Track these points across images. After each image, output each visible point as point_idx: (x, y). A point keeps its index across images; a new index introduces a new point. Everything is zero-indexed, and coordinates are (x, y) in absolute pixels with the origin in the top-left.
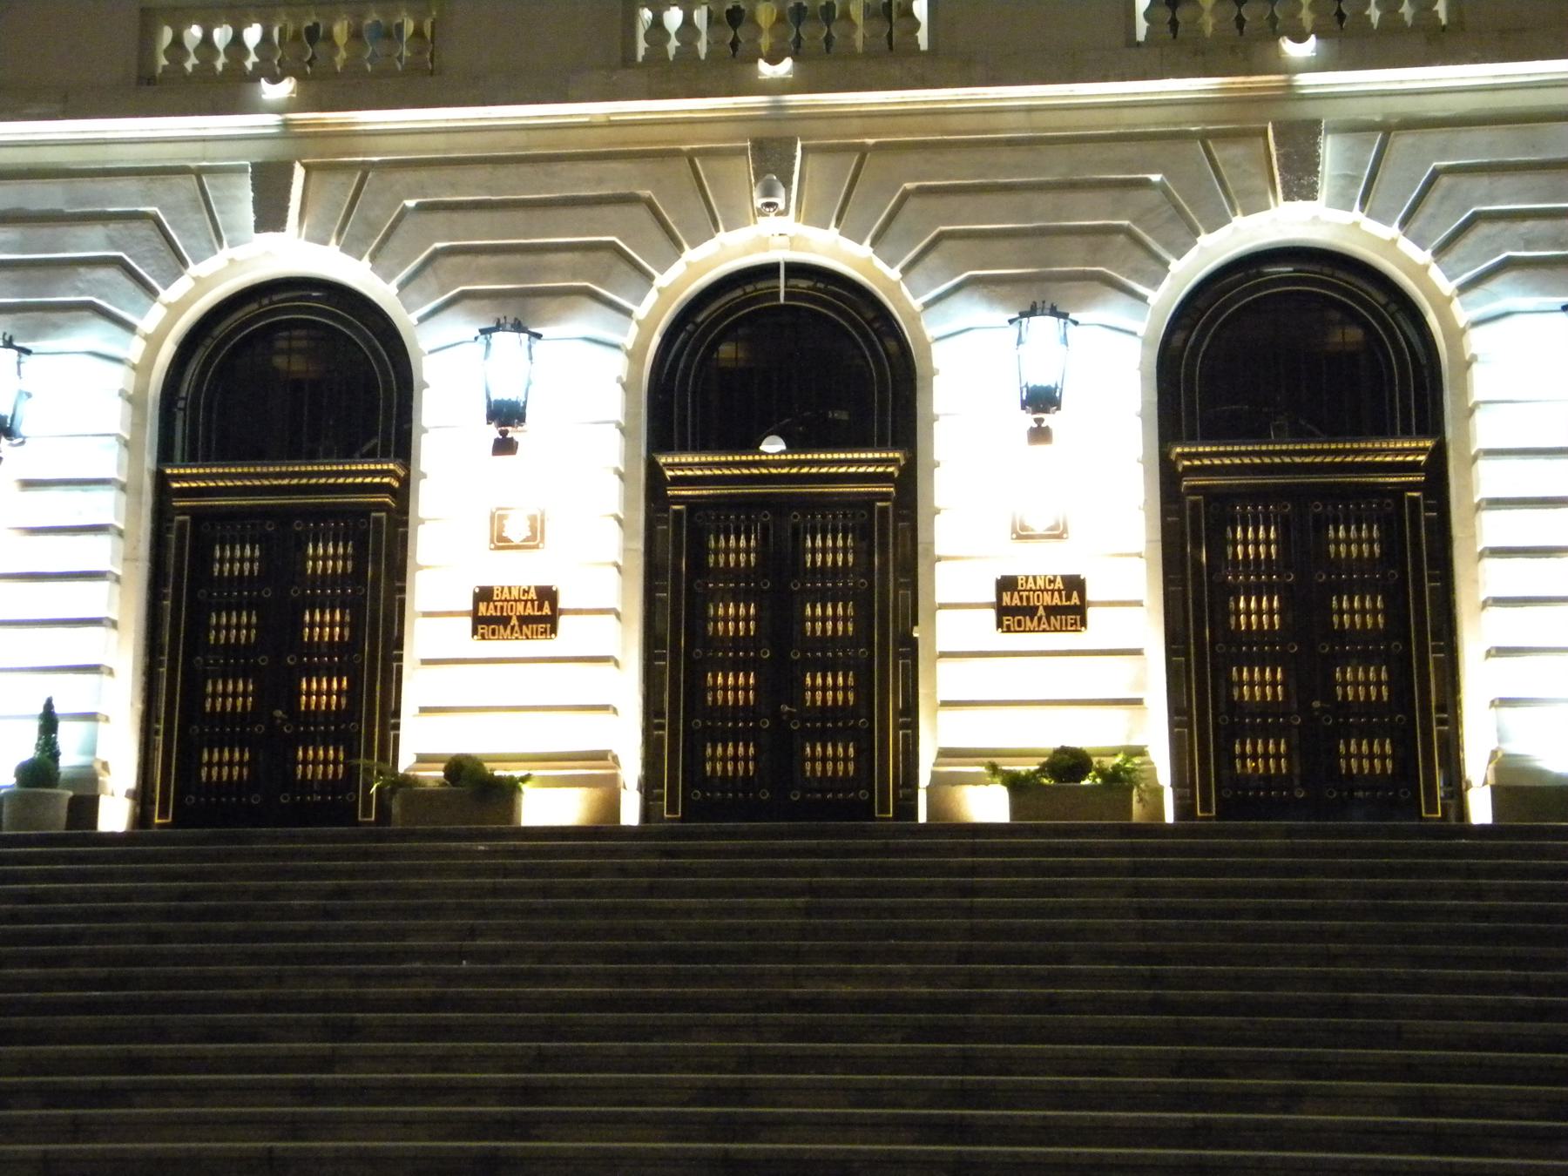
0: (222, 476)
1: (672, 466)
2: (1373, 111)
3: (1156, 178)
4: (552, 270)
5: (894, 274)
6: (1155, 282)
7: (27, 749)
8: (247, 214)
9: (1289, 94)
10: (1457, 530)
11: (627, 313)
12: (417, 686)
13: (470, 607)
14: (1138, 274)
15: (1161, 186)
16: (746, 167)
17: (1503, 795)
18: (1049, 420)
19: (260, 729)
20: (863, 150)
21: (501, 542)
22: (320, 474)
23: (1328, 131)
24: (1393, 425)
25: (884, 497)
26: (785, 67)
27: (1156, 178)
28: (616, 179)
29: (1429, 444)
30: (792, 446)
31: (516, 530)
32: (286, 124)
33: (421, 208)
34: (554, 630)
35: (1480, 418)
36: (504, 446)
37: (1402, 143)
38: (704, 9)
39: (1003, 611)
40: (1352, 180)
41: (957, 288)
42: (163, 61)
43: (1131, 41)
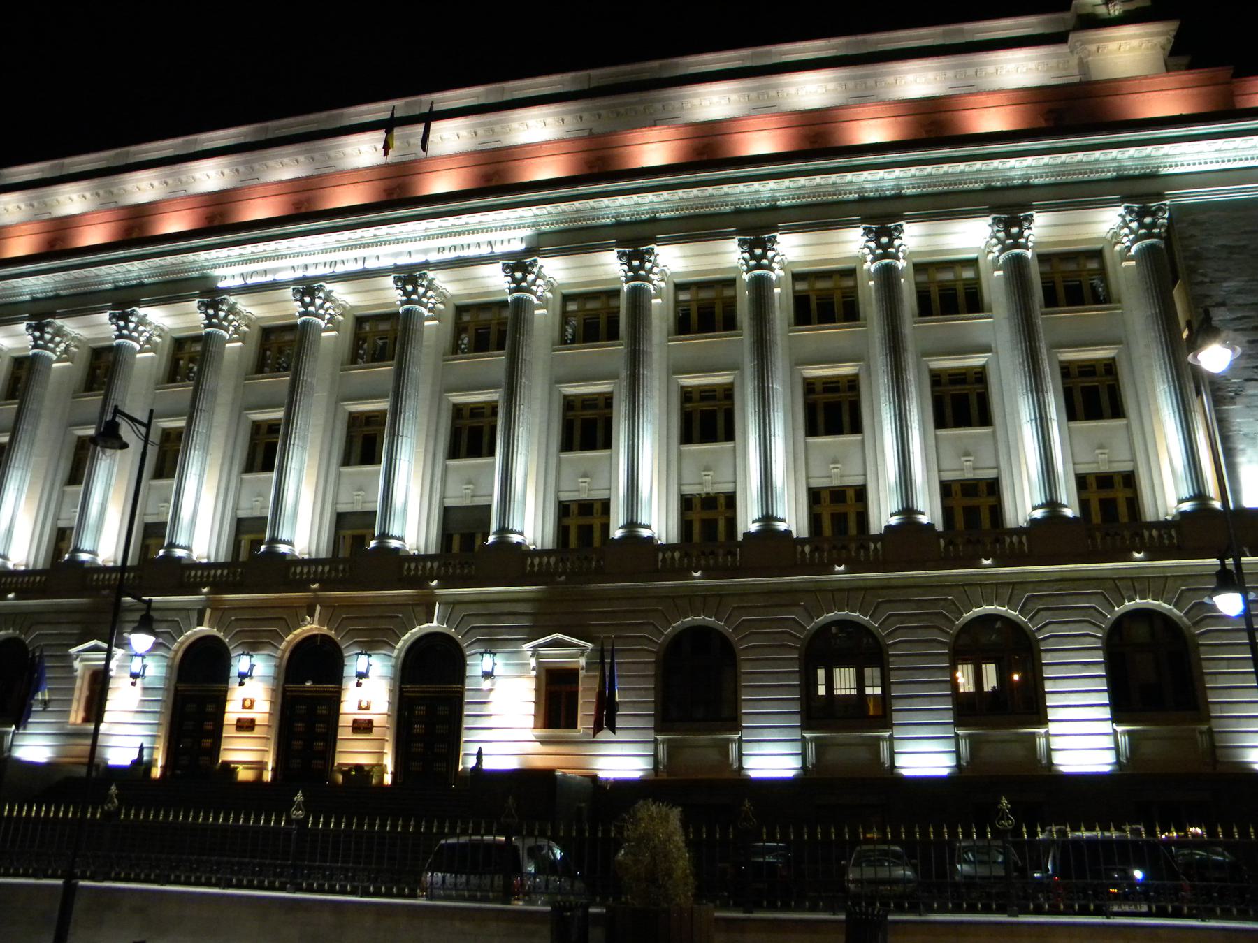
2: (451, 599)
7: (135, 757)
8: (196, 622)
12: (340, 747)
18: (363, 681)
20: (335, 606)
21: (244, 707)
26: (842, 568)
30: (314, 683)
31: (364, 705)
32: (208, 598)
33: (236, 620)
37: (457, 607)
42: (405, 573)
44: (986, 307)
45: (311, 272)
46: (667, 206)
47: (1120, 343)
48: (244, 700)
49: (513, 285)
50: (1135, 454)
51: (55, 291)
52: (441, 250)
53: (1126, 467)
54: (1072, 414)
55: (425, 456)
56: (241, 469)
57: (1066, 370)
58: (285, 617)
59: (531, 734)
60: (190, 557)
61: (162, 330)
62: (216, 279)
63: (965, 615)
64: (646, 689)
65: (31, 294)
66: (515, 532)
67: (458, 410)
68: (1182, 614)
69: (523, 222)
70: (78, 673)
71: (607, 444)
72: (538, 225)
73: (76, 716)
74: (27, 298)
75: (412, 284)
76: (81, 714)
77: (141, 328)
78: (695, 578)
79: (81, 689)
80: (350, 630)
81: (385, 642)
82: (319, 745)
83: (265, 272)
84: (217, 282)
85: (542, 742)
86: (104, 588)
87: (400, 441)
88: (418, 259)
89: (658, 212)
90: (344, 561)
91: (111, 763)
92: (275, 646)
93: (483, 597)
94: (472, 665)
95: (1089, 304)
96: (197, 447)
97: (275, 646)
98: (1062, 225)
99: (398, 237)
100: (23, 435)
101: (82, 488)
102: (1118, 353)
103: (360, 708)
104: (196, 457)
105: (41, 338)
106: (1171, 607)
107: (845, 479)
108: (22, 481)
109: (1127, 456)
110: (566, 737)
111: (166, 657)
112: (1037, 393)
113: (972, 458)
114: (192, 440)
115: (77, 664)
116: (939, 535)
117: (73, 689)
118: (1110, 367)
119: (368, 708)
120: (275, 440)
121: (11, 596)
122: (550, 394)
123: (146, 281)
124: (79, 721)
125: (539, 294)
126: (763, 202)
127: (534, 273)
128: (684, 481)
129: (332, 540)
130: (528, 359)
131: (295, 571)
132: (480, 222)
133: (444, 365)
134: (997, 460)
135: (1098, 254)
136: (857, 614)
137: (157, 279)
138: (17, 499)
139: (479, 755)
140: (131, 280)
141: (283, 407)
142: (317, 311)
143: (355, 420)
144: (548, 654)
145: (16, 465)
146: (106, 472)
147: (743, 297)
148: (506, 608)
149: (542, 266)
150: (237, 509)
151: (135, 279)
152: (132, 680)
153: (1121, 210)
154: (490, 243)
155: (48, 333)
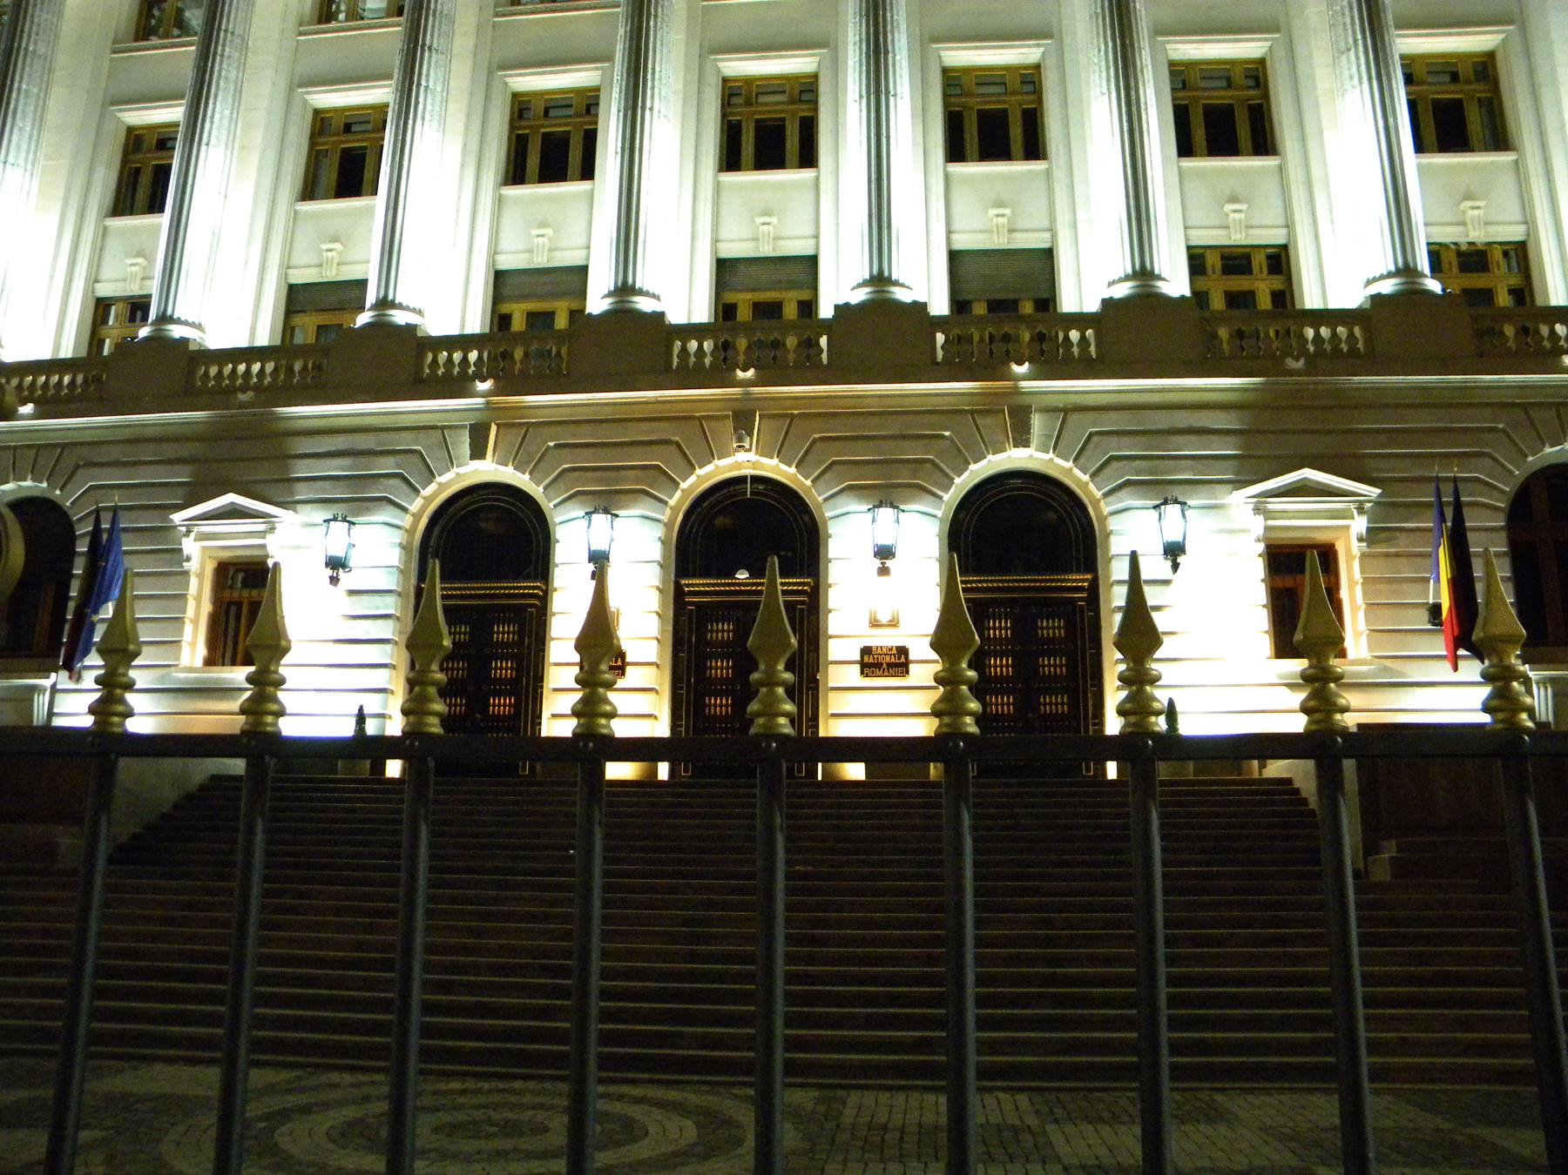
0: (718, 585)
1: (688, 586)
2: (1059, 402)
3: (947, 434)
5: (808, 483)
6: (946, 490)
9: (1017, 391)
10: (1103, 624)
11: (665, 503)
14: (936, 484)
20: (792, 417)
25: (802, 603)
26: (751, 373)
27: (947, 434)
29: (1089, 577)
32: (488, 403)
37: (1074, 418)
50: (1292, 215)
53: (1276, 237)
56: (500, 178)
57: (1182, 76)
67: (521, 106)
70: (192, 566)
76: (202, 651)
79: (198, 599)
80: (834, 463)
82: (501, 705)
86: (244, 389)
90: (304, 351)
91: (617, 735)
92: (934, 495)
96: (427, 117)
97: (934, 495)
100: (21, 102)
101: (164, 220)
107: (783, 243)
113: (1007, 211)
114: (417, 103)
115: (190, 546)
116: (939, 323)
118: (1256, 74)
119: (894, 623)
120: (594, 127)
122: (289, 102)
124: (199, 662)
128: (295, 261)
131: (206, 373)
133: (112, 60)
143: (135, 140)
148: (1181, 419)
152: (329, 572)
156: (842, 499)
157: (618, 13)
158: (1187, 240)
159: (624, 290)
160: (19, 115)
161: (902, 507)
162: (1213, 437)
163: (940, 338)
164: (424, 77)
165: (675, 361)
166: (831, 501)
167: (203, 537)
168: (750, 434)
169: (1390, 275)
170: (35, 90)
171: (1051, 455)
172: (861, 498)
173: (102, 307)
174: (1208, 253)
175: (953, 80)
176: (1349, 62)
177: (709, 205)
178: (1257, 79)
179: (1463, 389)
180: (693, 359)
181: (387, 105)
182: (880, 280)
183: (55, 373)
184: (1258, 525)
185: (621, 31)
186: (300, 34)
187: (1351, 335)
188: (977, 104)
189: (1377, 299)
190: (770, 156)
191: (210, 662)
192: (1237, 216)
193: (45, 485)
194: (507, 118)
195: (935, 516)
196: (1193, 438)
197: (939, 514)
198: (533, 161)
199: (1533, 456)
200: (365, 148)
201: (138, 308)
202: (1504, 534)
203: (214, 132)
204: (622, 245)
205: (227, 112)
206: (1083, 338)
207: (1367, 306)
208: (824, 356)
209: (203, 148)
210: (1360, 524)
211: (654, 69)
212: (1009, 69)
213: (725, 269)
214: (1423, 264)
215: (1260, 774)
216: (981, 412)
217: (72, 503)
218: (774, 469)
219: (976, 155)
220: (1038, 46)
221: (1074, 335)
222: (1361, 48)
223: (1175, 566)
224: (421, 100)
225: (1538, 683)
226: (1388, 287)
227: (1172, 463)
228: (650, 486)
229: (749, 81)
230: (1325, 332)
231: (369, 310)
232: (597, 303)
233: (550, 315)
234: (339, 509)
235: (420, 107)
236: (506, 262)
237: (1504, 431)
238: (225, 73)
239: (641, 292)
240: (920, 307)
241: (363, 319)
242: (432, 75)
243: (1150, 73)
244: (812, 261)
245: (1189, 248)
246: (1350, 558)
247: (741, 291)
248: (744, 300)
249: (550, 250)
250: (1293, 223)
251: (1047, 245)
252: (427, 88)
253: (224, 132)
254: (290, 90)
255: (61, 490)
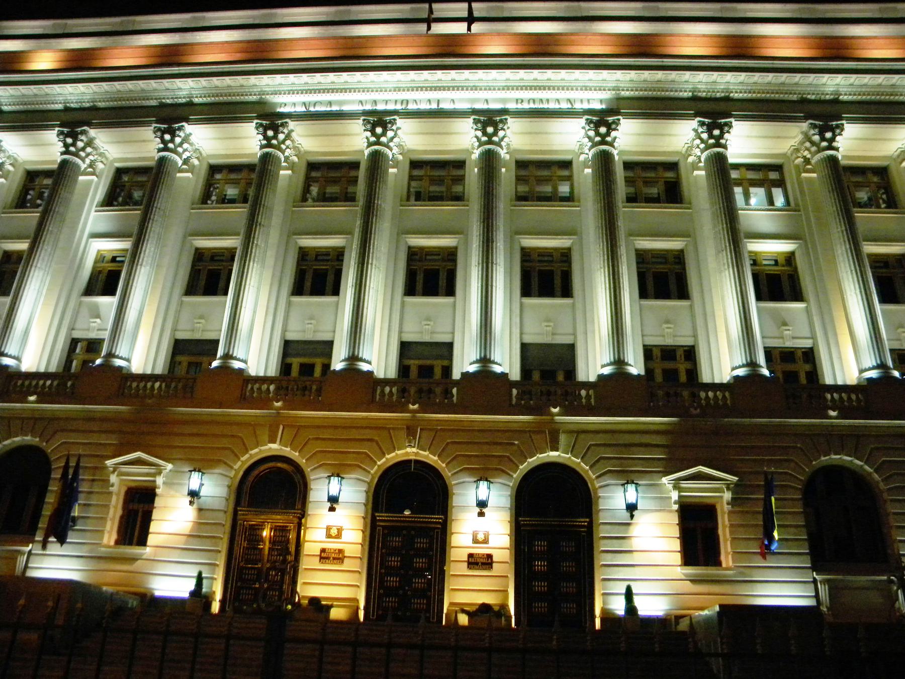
0: (395, 517)
1: (379, 516)
2: (572, 427)
3: (516, 442)
4: (636, 466)
5: (444, 465)
6: (515, 472)
9: (553, 422)
10: (595, 545)
11: (369, 472)
12: (449, 584)
13: (319, 553)
14: (510, 470)
15: (518, 445)
16: (403, 434)
17: (603, 620)
19: (401, 592)
20: (437, 431)
22: (426, 518)
23: (562, 432)
24: (382, 508)
25: (438, 528)
26: (416, 406)
27: (516, 442)
28: (368, 434)
29: (588, 520)
31: (481, 537)
34: (343, 562)
35: (601, 514)
36: (481, 514)
37: (582, 436)
38: (396, 388)
39: (321, 558)
40: (568, 445)
41: (461, 470)
43: (511, 405)
44: (576, 198)
45: (381, 107)
46: (741, 88)
47: (689, 236)
48: (328, 529)
49: (264, 142)
50: (696, 330)
51: (92, 102)
52: (520, 101)
53: (688, 342)
54: (644, 294)
55: (271, 288)
56: (183, 291)
57: (642, 257)
58: (376, 438)
59: (680, 572)
60: (128, 369)
61: (16, 160)
62: (275, 105)
63: (521, 467)
64: (797, 526)
65: (64, 103)
66: (496, 363)
67: (303, 254)
68: (872, 471)
69: (604, 85)
71: (336, 292)
72: (619, 90)
73: (110, 536)
74: (60, 107)
75: (170, 134)
77: (185, 146)
78: (831, 418)
81: (503, 471)
83: (330, 103)
84: (276, 108)
85: (691, 581)
87: (138, 271)
88: (391, 107)
89: (732, 92)
91: (157, 593)
93: (609, 427)
94: (604, 498)
95: (664, 203)
96: (256, 260)
97: (509, 475)
98: (867, 139)
99: (476, 85)
100: (48, 236)
102: (686, 245)
103: (475, 541)
104: (254, 270)
105: (74, 145)
106: (436, 458)
107: (435, 335)
108: (43, 282)
109: (689, 332)
110: (718, 575)
111: (226, 476)
112: (738, 267)
113: (552, 324)
115: (113, 478)
116: (515, 384)
117: (107, 506)
118: (679, 257)
121: (32, 398)
123: (196, 100)
124: (112, 543)
125: (286, 154)
126: (718, 92)
127: (284, 133)
128: (179, 327)
129: (169, 361)
130: (163, 208)
132: (293, 84)
134: (575, 328)
135: (673, 166)
136: (579, 461)
137: (111, 104)
138: (37, 300)
139: (629, 594)
140: (180, 98)
141: (28, 239)
142: (388, 143)
144: (690, 488)
145: (39, 265)
146: (146, 278)
147: (473, 173)
148: (637, 439)
149: (398, 128)
150: (286, 331)
151: (184, 98)
153: (805, 125)
154: (569, 101)
155: (82, 140)
156: (460, 475)
157: (357, 210)
158: (643, 341)
159: (353, 358)
160: (46, 243)
161: (492, 480)
162: (654, 449)
163: (515, 391)
164: (256, 239)
165: (378, 397)
166: (456, 475)
167: (121, 474)
168: (415, 438)
169: (743, 366)
170: (56, 231)
171: (569, 455)
172: (471, 475)
173: (74, 342)
174: (654, 349)
175: (526, 255)
176: (723, 257)
177: (398, 314)
178: (679, 258)
179: (780, 425)
180: (387, 397)
181: (236, 248)
182: (485, 360)
183: (48, 379)
184: (675, 495)
185: (358, 223)
186: (193, 209)
187: (724, 396)
188: (539, 266)
189: (737, 378)
190: (431, 290)
191: (117, 543)
192: (668, 330)
193: (38, 439)
194: (296, 260)
195: (509, 486)
196: (642, 449)
197: (511, 484)
198: (308, 284)
199: (815, 461)
200: (221, 270)
201: (93, 346)
202: (801, 502)
203: (145, 259)
204: (353, 335)
205: (153, 249)
206: (588, 394)
207: (732, 382)
208: (455, 399)
209: (139, 267)
210: (727, 496)
211: (374, 243)
212: (556, 249)
213: (405, 347)
214: (761, 359)
215: (676, 628)
216: (534, 432)
217: (52, 450)
218: (427, 457)
219: (537, 293)
220: (570, 239)
221: (583, 393)
222: (728, 250)
223: (632, 516)
224: (254, 251)
225: (821, 582)
226: (741, 372)
227: (630, 461)
228: (361, 463)
229: (422, 249)
230: (711, 394)
231: (219, 359)
232: (338, 364)
233: (312, 367)
234: (198, 466)
235: (253, 254)
236: (291, 336)
237: (800, 448)
238: (154, 228)
239: (362, 360)
240: (504, 375)
241: (215, 364)
242: (259, 239)
243: (625, 258)
244: (450, 346)
245: (644, 346)
246: (723, 513)
247: (412, 359)
248: (413, 363)
249: (314, 332)
250: (697, 335)
251: (571, 342)
252: (257, 245)
253: (150, 259)
254: (185, 237)
255: (47, 442)
